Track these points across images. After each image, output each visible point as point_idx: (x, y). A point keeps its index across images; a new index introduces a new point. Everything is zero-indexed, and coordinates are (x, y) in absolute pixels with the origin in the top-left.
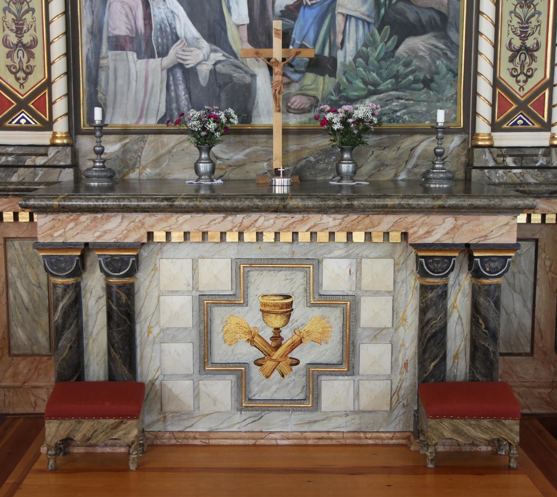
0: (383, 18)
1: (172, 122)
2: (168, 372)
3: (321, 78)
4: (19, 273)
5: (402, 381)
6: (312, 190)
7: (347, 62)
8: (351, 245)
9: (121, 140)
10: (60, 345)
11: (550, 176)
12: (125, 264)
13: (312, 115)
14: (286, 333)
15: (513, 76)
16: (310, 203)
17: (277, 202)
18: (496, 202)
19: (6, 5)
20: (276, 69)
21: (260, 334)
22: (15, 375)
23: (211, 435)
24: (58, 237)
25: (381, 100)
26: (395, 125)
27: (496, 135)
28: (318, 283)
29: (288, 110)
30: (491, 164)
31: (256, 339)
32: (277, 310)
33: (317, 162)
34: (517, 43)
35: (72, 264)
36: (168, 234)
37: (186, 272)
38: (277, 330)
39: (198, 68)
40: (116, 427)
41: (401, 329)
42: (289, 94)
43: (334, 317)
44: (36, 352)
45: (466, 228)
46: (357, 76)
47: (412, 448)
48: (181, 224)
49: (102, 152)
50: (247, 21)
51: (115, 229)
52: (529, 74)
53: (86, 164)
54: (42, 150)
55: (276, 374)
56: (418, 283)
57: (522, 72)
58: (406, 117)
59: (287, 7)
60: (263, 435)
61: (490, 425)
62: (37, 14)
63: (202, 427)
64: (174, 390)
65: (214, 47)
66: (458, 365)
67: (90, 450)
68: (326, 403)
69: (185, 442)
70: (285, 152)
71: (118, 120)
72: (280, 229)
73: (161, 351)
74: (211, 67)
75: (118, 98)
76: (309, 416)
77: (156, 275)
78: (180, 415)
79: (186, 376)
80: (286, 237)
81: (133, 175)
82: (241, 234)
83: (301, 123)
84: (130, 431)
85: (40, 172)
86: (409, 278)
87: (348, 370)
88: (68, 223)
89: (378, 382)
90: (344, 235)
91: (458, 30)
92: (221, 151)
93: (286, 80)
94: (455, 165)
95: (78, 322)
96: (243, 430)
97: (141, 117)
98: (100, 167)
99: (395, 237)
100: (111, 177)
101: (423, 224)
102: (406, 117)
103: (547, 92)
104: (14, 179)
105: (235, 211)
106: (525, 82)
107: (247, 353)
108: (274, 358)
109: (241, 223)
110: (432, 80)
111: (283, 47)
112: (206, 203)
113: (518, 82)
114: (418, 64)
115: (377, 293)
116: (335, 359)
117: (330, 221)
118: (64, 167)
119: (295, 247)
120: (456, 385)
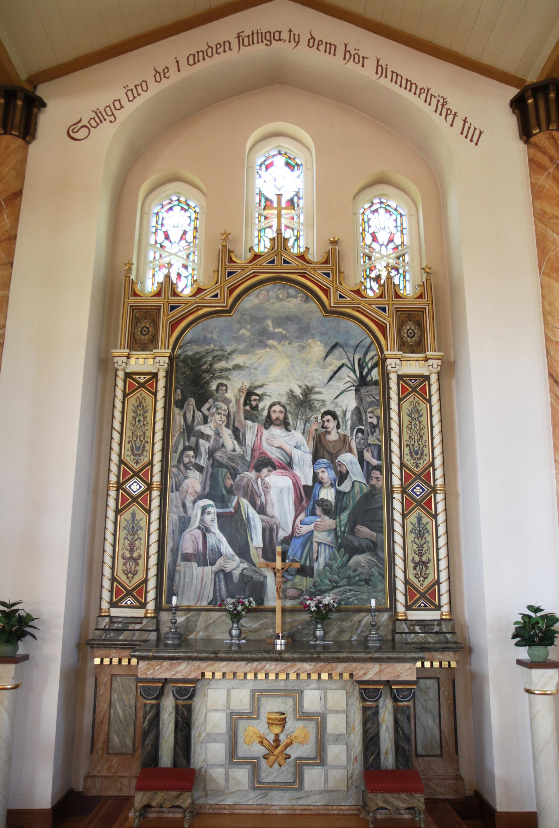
0: (340, 544)
1: (216, 604)
2: (210, 763)
3: (304, 579)
4: (118, 697)
5: (354, 770)
6: (299, 647)
7: (320, 569)
8: (320, 682)
9: (186, 615)
10: (146, 743)
11: (442, 638)
12: (187, 692)
13: (299, 600)
14: (282, 737)
15: (416, 578)
16: (296, 656)
17: (277, 655)
18: (402, 655)
19: (126, 536)
20: (278, 575)
21: (267, 738)
22: (109, 768)
23: (235, 807)
24: (150, 675)
25: (340, 591)
26: (349, 607)
27: (409, 613)
28: (301, 705)
29: (286, 597)
30: (407, 630)
31: (264, 741)
32: (277, 722)
33: (303, 629)
34: (417, 559)
35: (157, 691)
36: (213, 674)
37: (224, 698)
38: (277, 735)
39: (233, 572)
40: (177, 797)
41: (352, 735)
42: (286, 587)
43: (311, 727)
44: (124, 752)
45: (387, 670)
46: (326, 577)
47: (361, 816)
48: (222, 668)
49: (175, 623)
50: (262, 545)
51: (183, 670)
52: (425, 576)
53: (164, 629)
54: (139, 620)
55: (276, 765)
56: (361, 705)
57: (421, 576)
58: (355, 601)
59: (285, 538)
60: (268, 807)
61: (406, 798)
62: (142, 541)
63: (229, 801)
64: (213, 775)
65: (243, 560)
66: (388, 759)
67: (160, 815)
68: (307, 785)
69: (218, 811)
70: (283, 623)
71: (185, 603)
72: (279, 671)
73: (206, 748)
74: (240, 572)
75: (186, 589)
76: (296, 794)
77: (205, 700)
78: (218, 792)
79: (221, 766)
80: (282, 676)
81: (192, 636)
82: (256, 674)
83: (293, 605)
84: (186, 800)
85: (137, 634)
86: (355, 702)
87: (321, 762)
88: (156, 666)
89: (339, 771)
90: (316, 675)
91: (383, 551)
92: (246, 622)
93: (284, 579)
94: (385, 631)
95: (157, 728)
96: (255, 803)
97: (198, 601)
98: (173, 632)
99: (346, 676)
100: (180, 638)
101: (362, 668)
102: (355, 601)
103: (436, 587)
104: (121, 638)
105: (253, 660)
106: (424, 581)
107: (259, 750)
108: (275, 753)
109: (256, 667)
110: (370, 580)
111: (282, 561)
112: (236, 655)
113: (419, 581)
114: (361, 570)
115: (337, 712)
116: (312, 755)
117: (307, 666)
118: (151, 631)
119: (288, 683)
120: (387, 772)
